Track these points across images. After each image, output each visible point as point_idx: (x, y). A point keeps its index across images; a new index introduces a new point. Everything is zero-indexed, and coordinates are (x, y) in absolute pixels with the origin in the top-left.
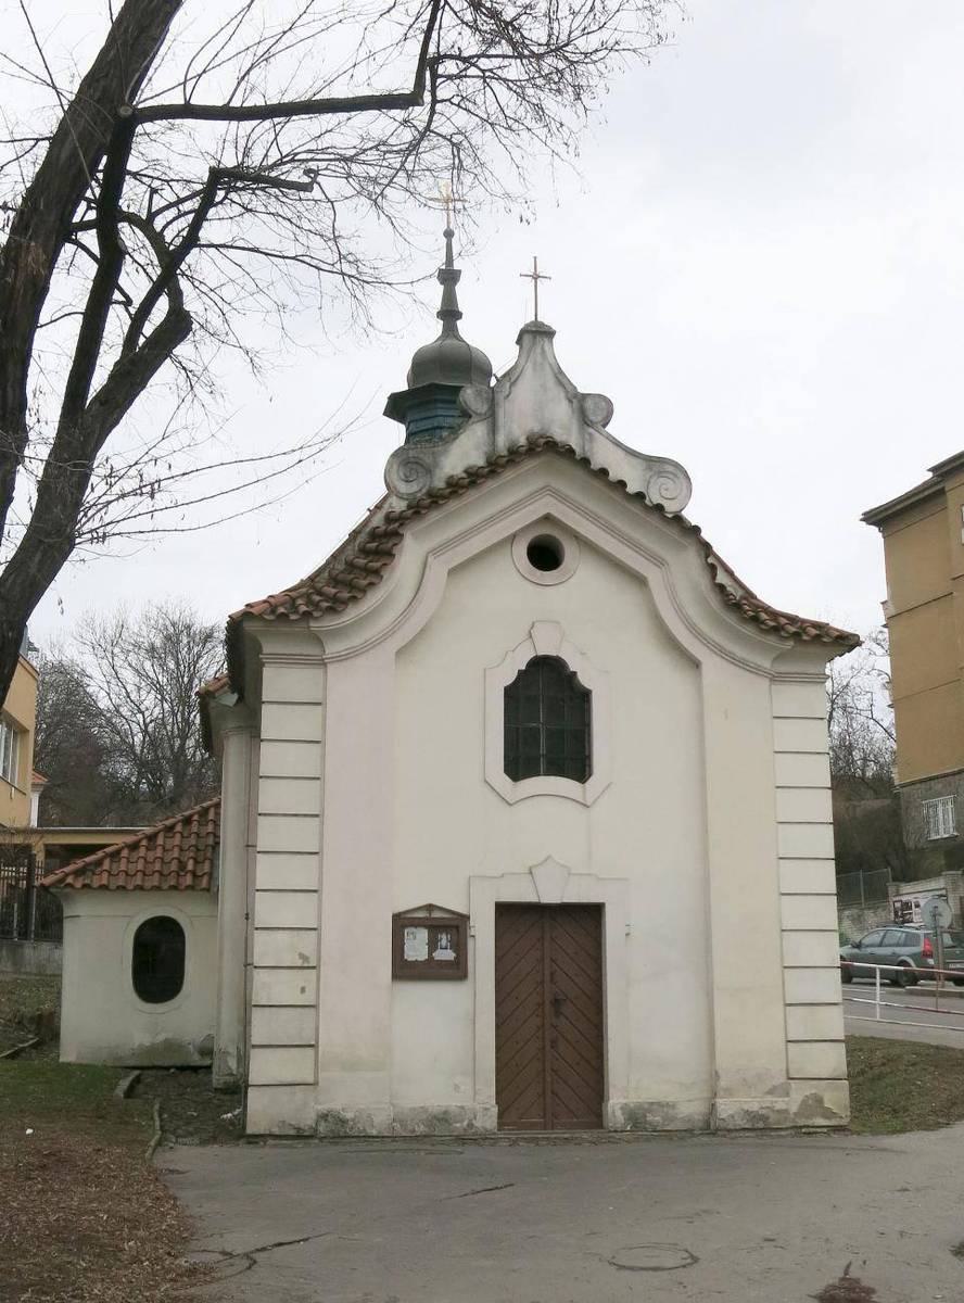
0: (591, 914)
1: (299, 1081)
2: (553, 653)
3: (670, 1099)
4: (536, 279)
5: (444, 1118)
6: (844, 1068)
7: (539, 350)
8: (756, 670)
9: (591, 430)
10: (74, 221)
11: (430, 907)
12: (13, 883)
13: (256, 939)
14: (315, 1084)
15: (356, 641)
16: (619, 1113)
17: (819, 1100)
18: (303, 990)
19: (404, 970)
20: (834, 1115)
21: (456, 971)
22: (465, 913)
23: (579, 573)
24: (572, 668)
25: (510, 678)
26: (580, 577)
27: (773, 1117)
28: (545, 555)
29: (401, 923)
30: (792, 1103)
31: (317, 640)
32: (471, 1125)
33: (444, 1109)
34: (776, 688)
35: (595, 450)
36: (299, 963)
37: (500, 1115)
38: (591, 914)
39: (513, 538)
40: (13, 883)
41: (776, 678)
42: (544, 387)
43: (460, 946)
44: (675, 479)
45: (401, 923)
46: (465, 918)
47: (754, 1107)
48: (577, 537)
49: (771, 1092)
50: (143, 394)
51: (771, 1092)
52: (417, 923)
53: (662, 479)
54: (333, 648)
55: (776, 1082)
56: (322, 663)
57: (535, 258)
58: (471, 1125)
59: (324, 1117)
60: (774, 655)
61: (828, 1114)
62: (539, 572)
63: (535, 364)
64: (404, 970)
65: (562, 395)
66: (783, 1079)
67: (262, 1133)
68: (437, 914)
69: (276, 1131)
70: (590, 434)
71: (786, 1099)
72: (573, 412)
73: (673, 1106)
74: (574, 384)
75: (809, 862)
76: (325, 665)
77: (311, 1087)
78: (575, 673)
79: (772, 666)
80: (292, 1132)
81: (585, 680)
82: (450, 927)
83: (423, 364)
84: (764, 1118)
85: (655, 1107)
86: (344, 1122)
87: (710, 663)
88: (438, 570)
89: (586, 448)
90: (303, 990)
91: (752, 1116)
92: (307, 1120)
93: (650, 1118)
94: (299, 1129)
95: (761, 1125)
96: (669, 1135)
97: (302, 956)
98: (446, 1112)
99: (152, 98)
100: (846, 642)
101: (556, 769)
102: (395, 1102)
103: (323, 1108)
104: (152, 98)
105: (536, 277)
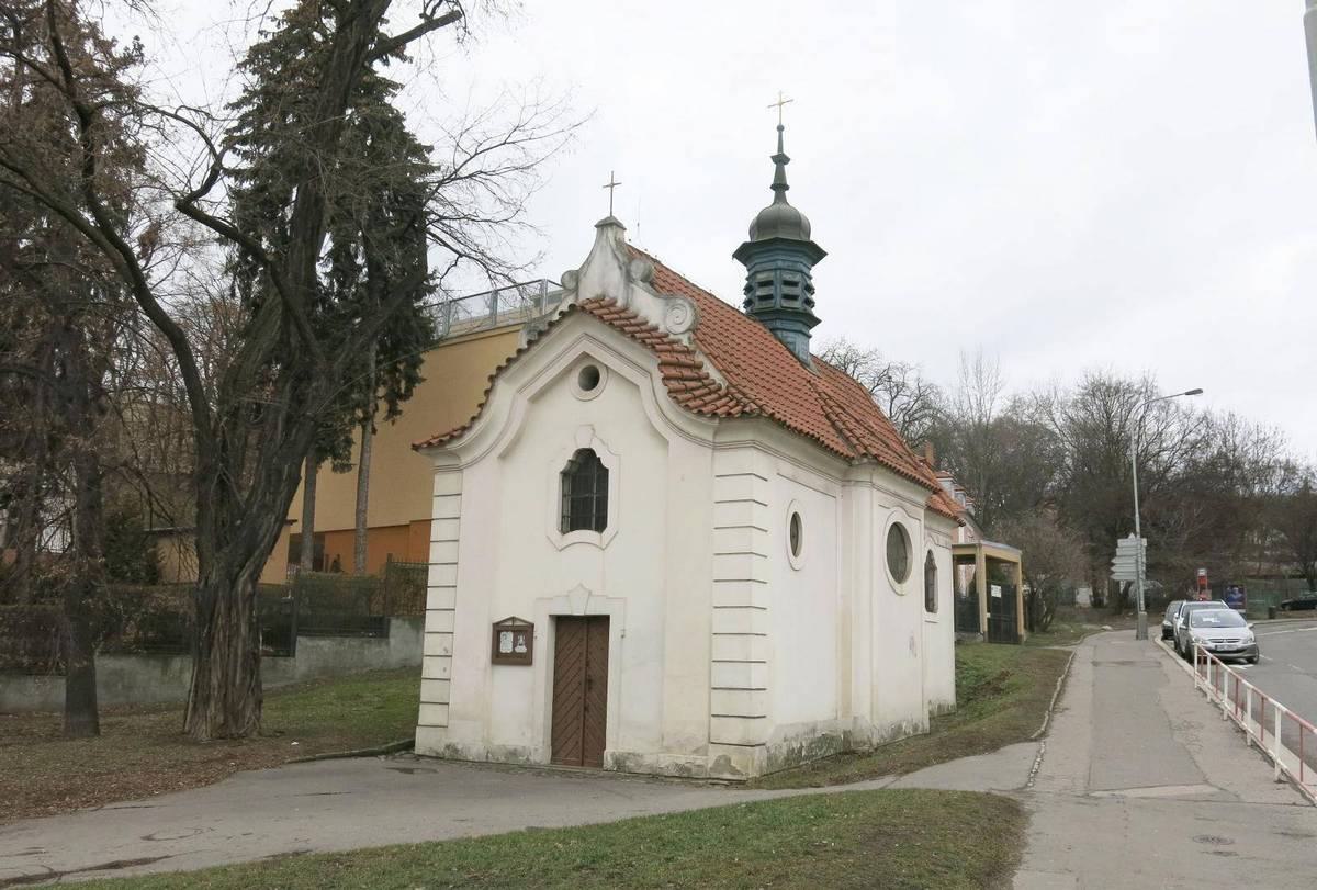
0: (603, 620)
3: (640, 751)
5: (514, 753)
8: (701, 442)
13: (426, 640)
15: (477, 453)
16: (609, 759)
17: (728, 760)
18: (445, 670)
19: (498, 658)
20: (738, 772)
21: (525, 660)
23: (608, 388)
27: (694, 770)
28: (591, 379)
29: (498, 629)
30: (709, 760)
32: (528, 759)
34: (717, 454)
37: (554, 754)
38: (603, 620)
39: (567, 371)
41: (716, 447)
42: (606, 264)
43: (529, 644)
45: (498, 629)
46: (532, 626)
47: (682, 761)
49: (696, 751)
51: (696, 751)
52: (507, 629)
54: (465, 459)
55: (700, 745)
56: (459, 469)
58: (528, 759)
59: (448, 747)
61: (734, 771)
64: (498, 658)
65: (616, 265)
66: (705, 742)
68: (518, 623)
69: (427, 753)
71: (704, 758)
73: (642, 756)
79: (714, 438)
80: (434, 755)
82: (525, 631)
83: (762, 224)
84: (689, 770)
85: (631, 756)
86: (456, 750)
87: (675, 440)
88: (523, 401)
90: (445, 670)
91: (682, 768)
92: (441, 748)
93: (628, 763)
94: (437, 753)
95: (685, 775)
96: (637, 775)
97: (446, 650)
98: (515, 750)
103: (448, 741)
105: (612, 185)
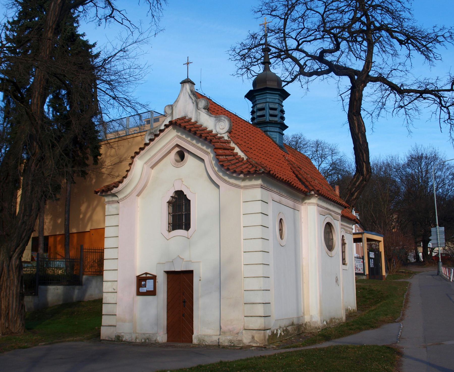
1: (113, 325)
4: (188, 64)
7: (185, 88)
9: (199, 111)
11: (146, 274)
21: (153, 293)
26: (258, 37)
29: (139, 293)
31: (114, 195)
33: (147, 335)
36: (113, 291)
44: (225, 122)
48: (189, 152)
54: (121, 196)
57: (188, 57)
60: (202, 127)
63: (184, 94)
72: (194, 106)
76: (119, 203)
78: (186, 195)
80: (110, 339)
89: (198, 118)
99: (343, 252)
100: (381, 241)
104: (343, 252)
105: (188, 64)
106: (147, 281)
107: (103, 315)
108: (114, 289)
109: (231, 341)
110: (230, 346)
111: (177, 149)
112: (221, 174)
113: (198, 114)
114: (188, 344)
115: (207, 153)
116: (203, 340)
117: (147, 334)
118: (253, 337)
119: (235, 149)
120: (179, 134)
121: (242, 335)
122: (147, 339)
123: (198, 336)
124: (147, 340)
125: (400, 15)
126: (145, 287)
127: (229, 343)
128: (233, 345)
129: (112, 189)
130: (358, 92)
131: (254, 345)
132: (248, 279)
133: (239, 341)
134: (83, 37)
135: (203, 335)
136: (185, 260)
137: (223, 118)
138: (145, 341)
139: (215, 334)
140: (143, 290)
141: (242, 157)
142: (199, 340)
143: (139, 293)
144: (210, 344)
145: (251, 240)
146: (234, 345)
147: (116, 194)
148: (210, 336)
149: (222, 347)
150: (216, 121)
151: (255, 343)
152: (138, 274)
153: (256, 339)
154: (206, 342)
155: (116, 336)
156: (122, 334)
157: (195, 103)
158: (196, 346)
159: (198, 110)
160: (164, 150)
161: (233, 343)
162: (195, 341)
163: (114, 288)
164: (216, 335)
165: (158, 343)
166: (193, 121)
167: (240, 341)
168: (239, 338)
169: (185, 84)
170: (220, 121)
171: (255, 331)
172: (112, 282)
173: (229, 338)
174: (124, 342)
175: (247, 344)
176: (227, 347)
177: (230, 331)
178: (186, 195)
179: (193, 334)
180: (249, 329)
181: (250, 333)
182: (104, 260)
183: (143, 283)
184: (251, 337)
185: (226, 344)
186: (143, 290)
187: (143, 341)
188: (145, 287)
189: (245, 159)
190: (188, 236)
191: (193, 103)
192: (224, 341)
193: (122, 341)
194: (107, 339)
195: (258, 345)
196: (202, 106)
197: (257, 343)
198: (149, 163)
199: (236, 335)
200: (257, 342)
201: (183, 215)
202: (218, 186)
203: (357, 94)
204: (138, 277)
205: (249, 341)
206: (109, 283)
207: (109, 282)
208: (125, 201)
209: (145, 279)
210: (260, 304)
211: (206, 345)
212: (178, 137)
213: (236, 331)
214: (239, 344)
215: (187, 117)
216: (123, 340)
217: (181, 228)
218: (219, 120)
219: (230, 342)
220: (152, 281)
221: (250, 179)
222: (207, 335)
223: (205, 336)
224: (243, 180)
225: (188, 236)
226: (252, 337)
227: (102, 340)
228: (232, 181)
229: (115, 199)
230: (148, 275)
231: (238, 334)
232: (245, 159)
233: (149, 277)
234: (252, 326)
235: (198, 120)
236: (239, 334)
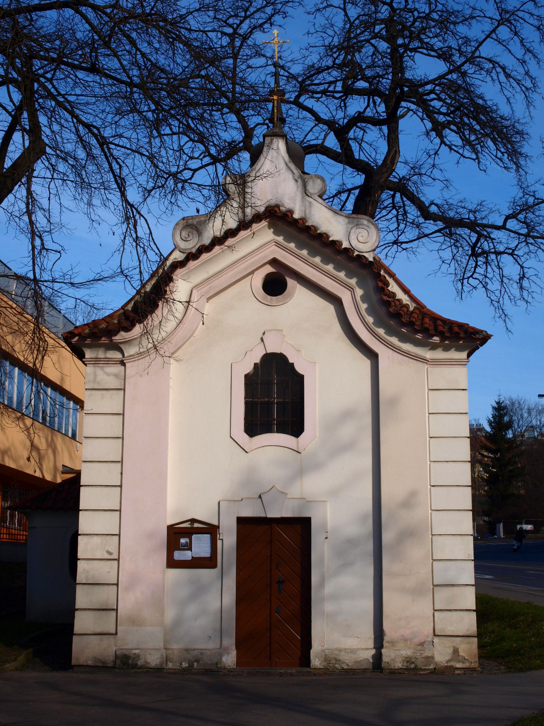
2: (278, 351)
6: (475, 628)
9: (311, 200)
10: (28, 129)
11: (193, 521)
12: (364, 67)
14: (116, 633)
17: (456, 651)
22: (215, 523)
24: (291, 361)
25: (249, 368)
29: (172, 563)
31: (117, 347)
35: (313, 213)
36: (107, 556)
40: (364, 67)
50: (472, 324)
53: (360, 230)
60: (430, 347)
62: (269, 297)
67: (82, 664)
70: (310, 203)
72: (298, 187)
74: (437, 76)
75: (451, 488)
77: (113, 636)
78: (293, 364)
80: (101, 665)
81: (299, 369)
89: (307, 212)
101: (282, 430)
102: (168, 647)
106: (194, 537)
107: (77, 610)
108: (110, 553)
109: (408, 660)
110: (407, 669)
111: (269, 269)
112: (381, 331)
113: (308, 204)
114: (307, 669)
115: (350, 288)
116: (336, 660)
117: (194, 650)
118: (456, 651)
119: (391, 286)
120: (280, 239)
121: (432, 646)
122: (196, 661)
123: (324, 651)
124: (195, 664)
125: (470, 85)
126: (190, 549)
127: (405, 664)
128: (413, 666)
129: (116, 333)
130: (373, 204)
131: (459, 665)
132: (441, 537)
133: (427, 658)
134: (455, 26)
135: (336, 649)
136: (288, 496)
137: (365, 222)
138: (191, 665)
139: (363, 647)
140: (178, 555)
141: (405, 302)
142: (327, 659)
143: (172, 563)
144: (354, 667)
145: (446, 464)
146: (416, 666)
147: (122, 346)
148: (353, 651)
149: (388, 671)
150: (350, 226)
151: (459, 662)
152: (170, 522)
153: (461, 654)
154: (344, 663)
155: (116, 656)
156: (137, 651)
157: (299, 181)
158: (319, 672)
159: (307, 197)
160: (243, 266)
161: (413, 663)
162: (316, 662)
163: (110, 550)
164: (367, 649)
165: (225, 668)
166: (296, 216)
167: (430, 659)
168: (427, 653)
169: (275, 140)
170: (357, 225)
171: (459, 639)
172: (104, 537)
173: (407, 652)
174: (140, 668)
175: (442, 664)
176: (400, 671)
177: (406, 640)
178: (293, 364)
179: (311, 648)
180: (445, 636)
181: (449, 643)
182: (82, 488)
183: (183, 541)
184: (450, 651)
185: (399, 665)
186: (178, 555)
187: (185, 665)
188: (190, 549)
189: (411, 309)
190: (298, 447)
191: (296, 181)
192: (393, 660)
193: (135, 666)
194: (90, 663)
195: (467, 665)
196: (316, 191)
197: (463, 663)
198: (205, 289)
199: (419, 647)
200: (464, 660)
201: (272, 403)
202: (373, 356)
203: (370, 208)
204: (170, 528)
205: (448, 658)
206: (96, 540)
207: (95, 537)
208: (136, 363)
209: (189, 532)
210: (468, 587)
211: (343, 669)
212: (278, 244)
213: (417, 640)
214: (426, 665)
215: (283, 206)
216: (137, 664)
217: (270, 431)
218: (357, 225)
219: (408, 662)
220: (207, 538)
221: (447, 349)
222: (345, 649)
223: (340, 651)
224: (434, 347)
225: (298, 447)
226: (454, 650)
227: (75, 666)
228: (407, 347)
229: (116, 355)
230: (196, 525)
231: (422, 644)
232: (411, 309)
233: (198, 528)
234: (451, 629)
235: (308, 216)
236: (425, 646)
